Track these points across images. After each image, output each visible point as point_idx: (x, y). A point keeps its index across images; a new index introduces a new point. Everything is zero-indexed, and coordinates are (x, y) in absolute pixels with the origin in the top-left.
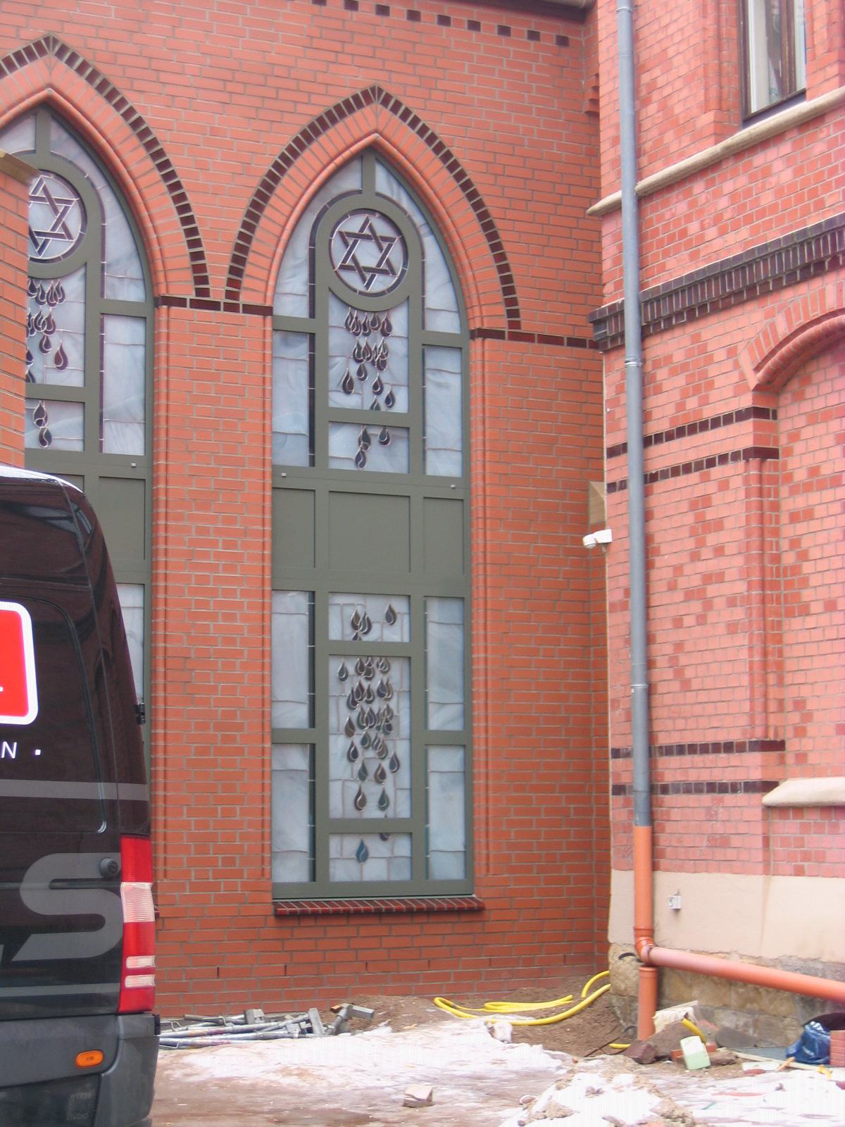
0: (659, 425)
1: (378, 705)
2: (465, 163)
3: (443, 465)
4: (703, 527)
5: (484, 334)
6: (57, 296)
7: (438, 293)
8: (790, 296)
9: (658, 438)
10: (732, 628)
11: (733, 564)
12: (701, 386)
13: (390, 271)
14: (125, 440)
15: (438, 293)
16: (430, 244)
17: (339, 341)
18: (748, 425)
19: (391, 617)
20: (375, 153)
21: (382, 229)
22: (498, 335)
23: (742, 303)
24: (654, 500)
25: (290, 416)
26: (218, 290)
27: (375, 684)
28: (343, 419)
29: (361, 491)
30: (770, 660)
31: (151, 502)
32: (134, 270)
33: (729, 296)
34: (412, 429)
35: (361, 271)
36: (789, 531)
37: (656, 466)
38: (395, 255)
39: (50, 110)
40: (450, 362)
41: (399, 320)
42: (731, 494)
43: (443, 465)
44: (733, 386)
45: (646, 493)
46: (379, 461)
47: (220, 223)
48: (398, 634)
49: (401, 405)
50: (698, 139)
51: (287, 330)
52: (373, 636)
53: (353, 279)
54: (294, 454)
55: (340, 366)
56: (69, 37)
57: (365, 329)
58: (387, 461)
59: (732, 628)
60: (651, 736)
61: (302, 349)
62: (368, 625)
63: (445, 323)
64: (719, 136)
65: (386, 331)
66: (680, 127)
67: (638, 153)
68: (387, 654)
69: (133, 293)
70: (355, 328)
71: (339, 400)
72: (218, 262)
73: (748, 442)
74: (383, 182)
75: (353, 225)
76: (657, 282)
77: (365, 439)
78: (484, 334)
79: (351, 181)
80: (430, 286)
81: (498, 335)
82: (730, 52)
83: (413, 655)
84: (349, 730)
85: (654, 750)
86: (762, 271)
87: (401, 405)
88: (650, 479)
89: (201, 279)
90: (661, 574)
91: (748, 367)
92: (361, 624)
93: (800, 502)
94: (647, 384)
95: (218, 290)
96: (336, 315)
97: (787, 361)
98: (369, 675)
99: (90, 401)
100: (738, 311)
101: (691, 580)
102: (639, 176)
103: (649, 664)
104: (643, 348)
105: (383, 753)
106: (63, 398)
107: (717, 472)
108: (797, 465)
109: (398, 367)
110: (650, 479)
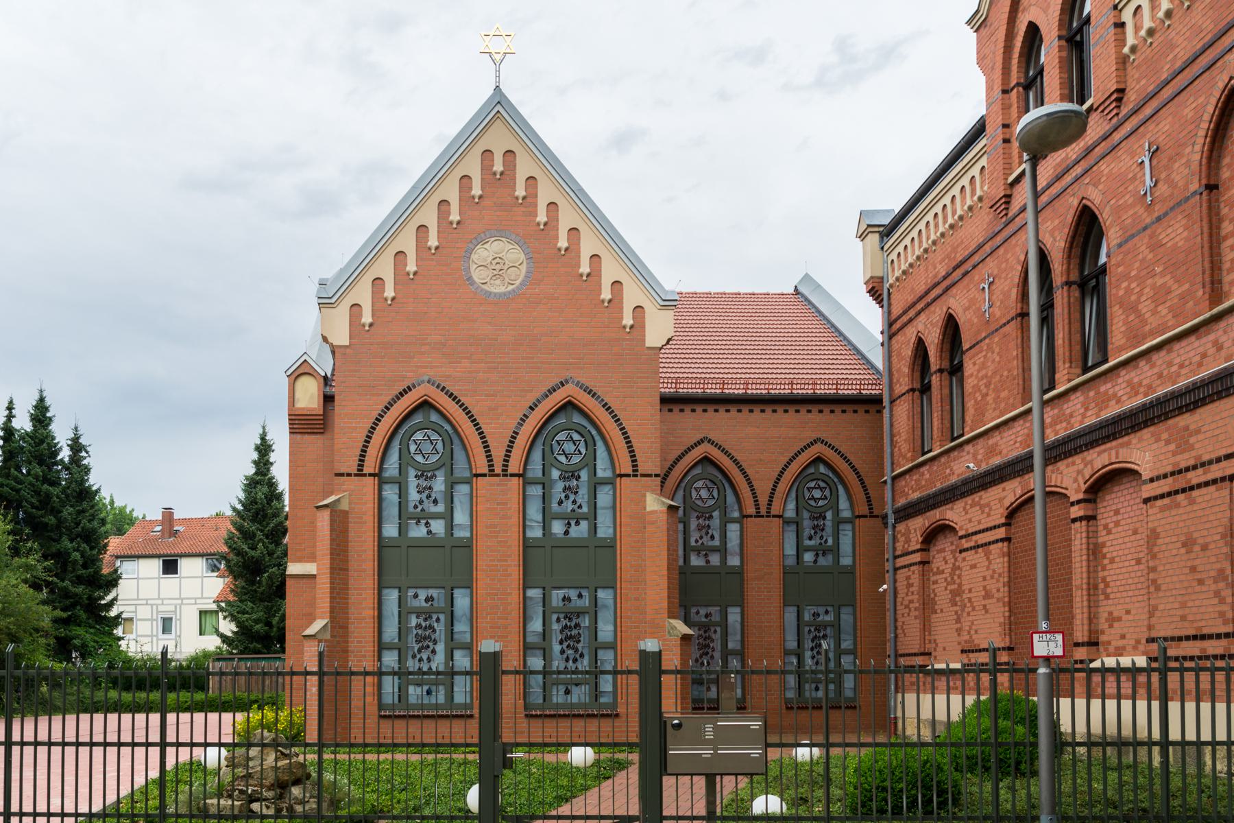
0: (898, 553)
1: (574, 632)
2: (852, 459)
3: (846, 561)
4: (909, 585)
5: (859, 517)
6: (711, 517)
7: (843, 504)
8: (1091, 455)
9: (899, 556)
10: (916, 617)
11: (916, 597)
12: (908, 541)
13: (826, 498)
14: (734, 561)
15: (843, 504)
16: (840, 488)
17: (807, 523)
18: (1003, 529)
19: (580, 596)
20: (818, 460)
21: (822, 484)
22: (865, 516)
23: (1213, 401)
24: (898, 577)
25: (790, 550)
26: (498, 470)
27: (573, 624)
28: (808, 549)
29: (815, 571)
30: (926, 627)
31: (742, 580)
32: (736, 507)
33: (1213, 394)
34: (835, 550)
35: (815, 500)
36: (932, 587)
37: (898, 565)
38: (827, 492)
39: (706, 460)
40: (849, 527)
41: (829, 515)
42: (915, 574)
43: (846, 561)
44: (915, 542)
45: (895, 574)
46: (822, 561)
47: (763, 489)
48: (829, 618)
49: (830, 542)
50: (908, 461)
51: (787, 522)
52: (572, 604)
53: (812, 503)
54: (791, 561)
55: (808, 531)
56: (711, 436)
57: (817, 518)
58: (581, 530)
59: (916, 617)
60: (896, 651)
61: (793, 527)
62: (819, 615)
63: (846, 514)
64: (913, 460)
65: (824, 518)
66: (904, 457)
67: (892, 464)
68: (826, 625)
69: (736, 514)
70: (813, 518)
71: (807, 543)
72: (763, 501)
73: (919, 559)
74: (822, 469)
75: (812, 484)
76: (1051, 437)
77: (817, 555)
78: (859, 517)
79: (812, 470)
80: (841, 502)
81: (865, 516)
82: (918, 432)
83: (836, 625)
84: (812, 649)
85: (897, 656)
86: (910, 511)
87: (830, 542)
88: (896, 569)
89: (757, 507)
90: (899, 600)
91: (1081, 482)
92: (816, 615)
93: (933, 578)
94: (895, 538)
95: (763, 511)
96: (806, 515)
97: (929, 534)
98: (570, 620)
99: (723, 550)
100: (1217, 404)
101: (906, 602)
102: (893, 471)
103: (896, 628)
104: (894, 527)
105: (576, 650)
106: (714, 550)
107: (912, 568)
108: (934, 566)
109: (583, 493)
110: (896, 569)
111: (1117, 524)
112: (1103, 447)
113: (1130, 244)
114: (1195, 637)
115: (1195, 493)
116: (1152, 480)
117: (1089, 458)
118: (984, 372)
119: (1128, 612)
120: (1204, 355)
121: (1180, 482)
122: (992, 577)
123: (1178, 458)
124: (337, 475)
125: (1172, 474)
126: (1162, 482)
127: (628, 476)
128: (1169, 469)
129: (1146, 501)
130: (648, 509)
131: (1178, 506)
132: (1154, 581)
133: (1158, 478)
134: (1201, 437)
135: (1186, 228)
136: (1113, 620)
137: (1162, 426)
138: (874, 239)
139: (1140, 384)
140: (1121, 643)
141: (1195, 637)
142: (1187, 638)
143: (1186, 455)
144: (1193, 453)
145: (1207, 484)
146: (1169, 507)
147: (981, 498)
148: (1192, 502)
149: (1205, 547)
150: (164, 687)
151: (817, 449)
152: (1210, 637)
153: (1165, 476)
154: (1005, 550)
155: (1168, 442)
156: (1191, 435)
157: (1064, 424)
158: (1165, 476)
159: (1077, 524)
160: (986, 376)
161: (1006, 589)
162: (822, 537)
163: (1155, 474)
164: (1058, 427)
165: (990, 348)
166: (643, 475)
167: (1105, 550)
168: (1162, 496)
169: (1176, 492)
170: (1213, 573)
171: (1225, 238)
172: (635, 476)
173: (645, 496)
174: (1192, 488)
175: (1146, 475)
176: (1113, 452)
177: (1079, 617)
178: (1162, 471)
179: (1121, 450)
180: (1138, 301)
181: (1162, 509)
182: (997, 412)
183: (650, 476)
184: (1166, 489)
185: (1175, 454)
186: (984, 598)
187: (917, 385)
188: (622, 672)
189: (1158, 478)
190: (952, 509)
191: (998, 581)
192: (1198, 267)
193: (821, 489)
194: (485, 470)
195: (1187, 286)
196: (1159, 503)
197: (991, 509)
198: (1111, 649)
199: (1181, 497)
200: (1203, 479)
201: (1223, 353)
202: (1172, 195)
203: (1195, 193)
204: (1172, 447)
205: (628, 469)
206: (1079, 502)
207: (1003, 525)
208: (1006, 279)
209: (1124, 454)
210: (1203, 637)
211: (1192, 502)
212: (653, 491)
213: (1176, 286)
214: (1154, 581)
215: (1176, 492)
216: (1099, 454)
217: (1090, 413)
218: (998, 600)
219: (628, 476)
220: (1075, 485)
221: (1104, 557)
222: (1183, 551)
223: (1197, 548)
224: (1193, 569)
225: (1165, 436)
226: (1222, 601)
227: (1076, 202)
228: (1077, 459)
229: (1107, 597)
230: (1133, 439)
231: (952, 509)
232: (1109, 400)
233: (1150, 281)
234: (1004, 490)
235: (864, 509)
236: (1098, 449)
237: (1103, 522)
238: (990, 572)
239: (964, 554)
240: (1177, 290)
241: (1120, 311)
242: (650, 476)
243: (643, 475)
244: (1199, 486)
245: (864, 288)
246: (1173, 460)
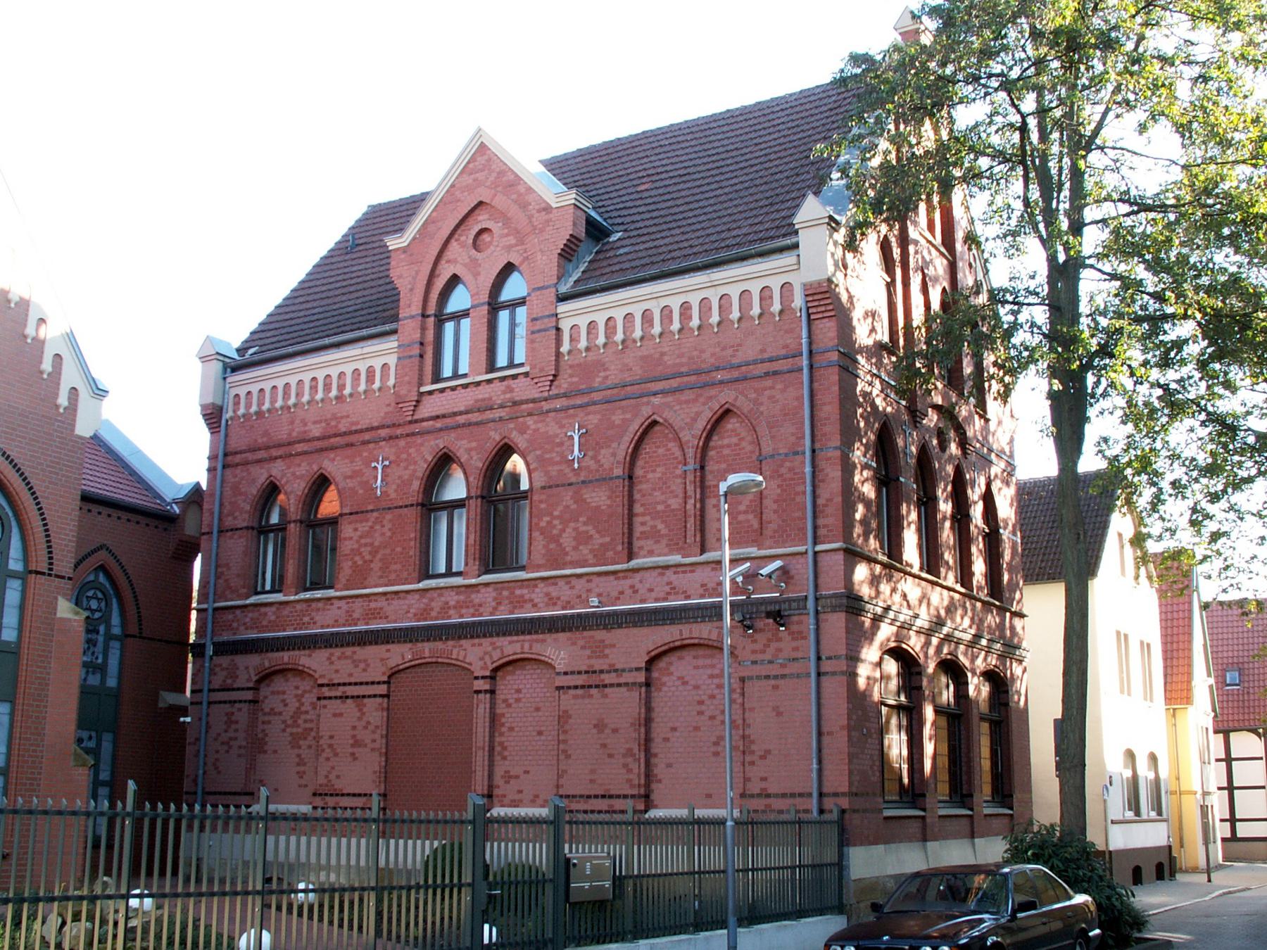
8: (502, 641)
13: (100, 611)
15: (116, 620)
21: (100, 595)
22: (134, 636)
36: (261, 727)
38: (103, 604)
63: (116, 631)
65: (98, 633)
74: (102, 578)
81: (134, 636)
88: (210, 703)
101: (225, 737)
111: (518, 700)
112: (515, 638)
113: (555, 490)
114: (603, 796)
115: (607, 690)
116: (566, 673)
117: (499, 644)
118: (368, 540)
119: (527, 772)
120: (622, 593)
121: (594, 679)
122: (366, 728)
123: (593, 661)
124: (1263, 787)
125: (587, 672)
126: (576, 676)
127: (43, 574)
128: (584, 668)
129: (559, 688)
130: (59, 615)
131: (591, 696)
132: (564, 751)
133: (572, 673)
134: (615, 650)
135: (610, 497)
136: (508, 777)
137: (578, 634)
138: (218, 366)
139: (559, 598)
140: (517, 797)
141: (603, 796)
142: (596, 797)
143: (601, 661)
144: (607, 661)
145: (619, 685)
146: (583, 697)
147: (354, 653)
148: (830, 733)
149: (615, 731)
150: (732, 920)
151: (103, 556)
152: (618, 796)
153: (579, 673)
154: (385, 705)
155: (583, 648)
156: (606, 646)
157: (472, 610)
158: (579, 673)
159: (481, 696)
160: (372, 544)
161: (384, 741)
162: (93, 653)
163: (569, 669)
164: (464, 611)
165: (378, 521)
166: (57, 576)
167: (503, 720)
168: (576, 687)
169: (590, 687)
170: (622, 751)
171: (637, 515)
172: (50, 575)
173: (56, 599)
174: (605, 686)
175: (560, 667)
176: (527, 646)
177: (479, 774)
178: (576, 669)
179: (535, 645)
180: (560, 535)
181: (575, 697)
182: (385, 580)
183: (63, 577)
184: (580, 683)
185: (589, 657)
186: (352, 746)
187: (256, 525)
188: (757, 870)
189: (572, 673)
190: (310, 656)
191: (374, 732)
192: (619, 528)
193: (98, 599)
194: (43, 567)
195: (607, 539)
196: (572, 692)
197: (368, 665)
198: (506, 801)
199: (594, 691)
200: (615, 681)
201: (638, 596)
202: (597, 471)
203: (618, 477)
204: (588, 652)
205: (43, 567)
206: (483, 677)
207: (384, 682)
208: (406, 468)
209: (537, 648)
210: (611, 797)
211: (606, 696)
212: (64, 595)
213: (597, 536)
214: (564, 751)
215: (590, 687)
216: (510, 643)
217: (502, 608)
218: (373, 750)
219: (43, 574)
220: (481, 663)
221: (503, 725)
222: (595, 731)
223: (607, 731)
224: (604, 746)
225: (581, 643)
226: (630, 771)
227: (498, 438)
228: (486, 642)
229: (504, 758)
230: (549, 638)
231: (310, 656)
232: (525, 601)
233: (572, 525)
234: (388, 651)
235: (133, 629)
236: (509, 638)
237: (502, 697)
238: (363, 723)
239: (323, 702)
240: (598, 540)
241: (541, 538)
242: (63, 577)
243: (57, 576)
244: (612, 685)
245: (197, 410)
246: (587, 662)
